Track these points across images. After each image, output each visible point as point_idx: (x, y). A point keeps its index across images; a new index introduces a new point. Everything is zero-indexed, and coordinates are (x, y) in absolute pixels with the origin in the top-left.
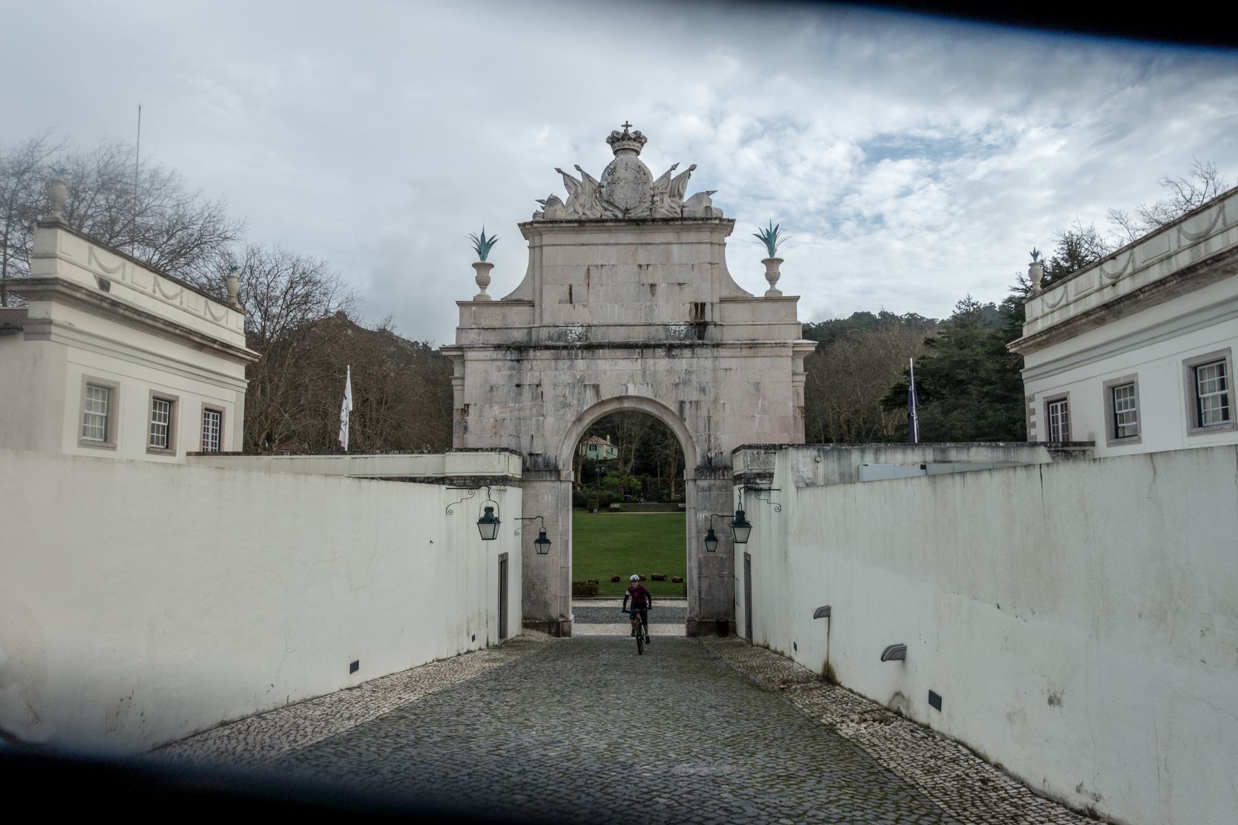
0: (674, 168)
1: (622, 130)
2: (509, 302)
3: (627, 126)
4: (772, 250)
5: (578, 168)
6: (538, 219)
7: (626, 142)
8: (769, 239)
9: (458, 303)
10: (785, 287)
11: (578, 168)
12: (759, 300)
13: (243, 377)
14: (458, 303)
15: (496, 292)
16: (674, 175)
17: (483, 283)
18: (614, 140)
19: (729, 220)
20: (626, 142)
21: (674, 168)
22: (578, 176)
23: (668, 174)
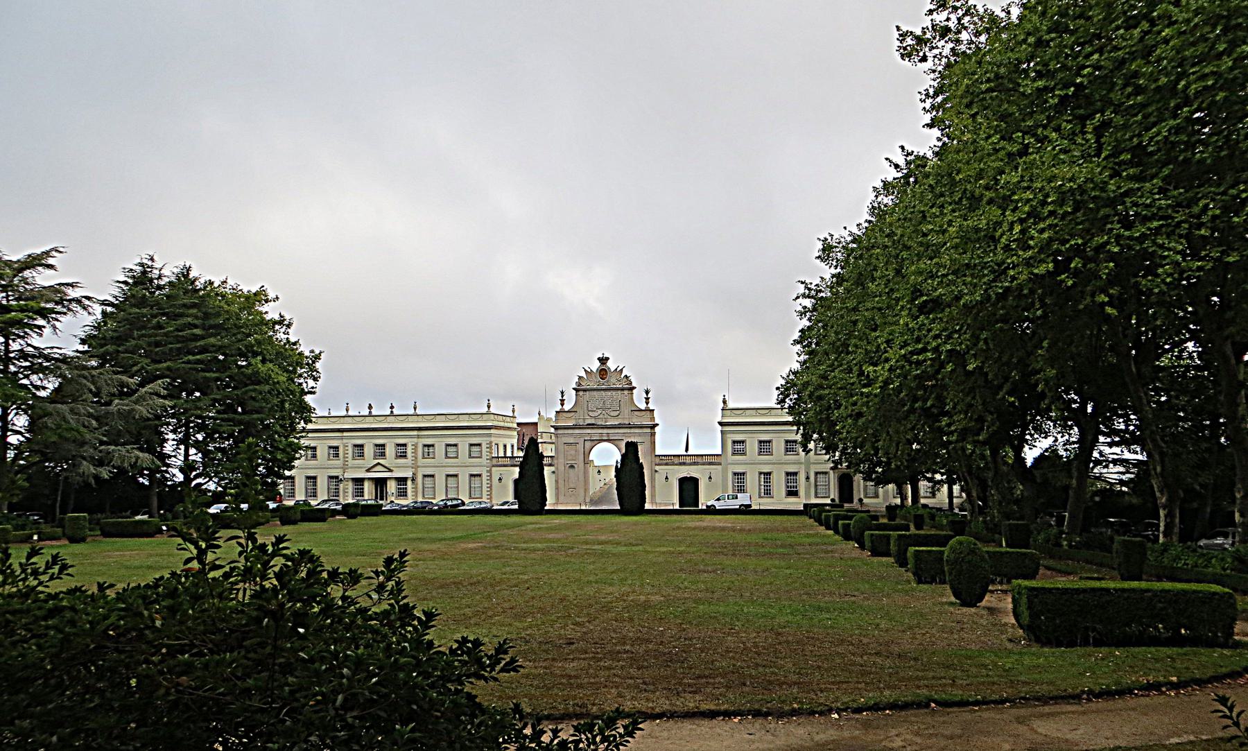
7: (603, 360)
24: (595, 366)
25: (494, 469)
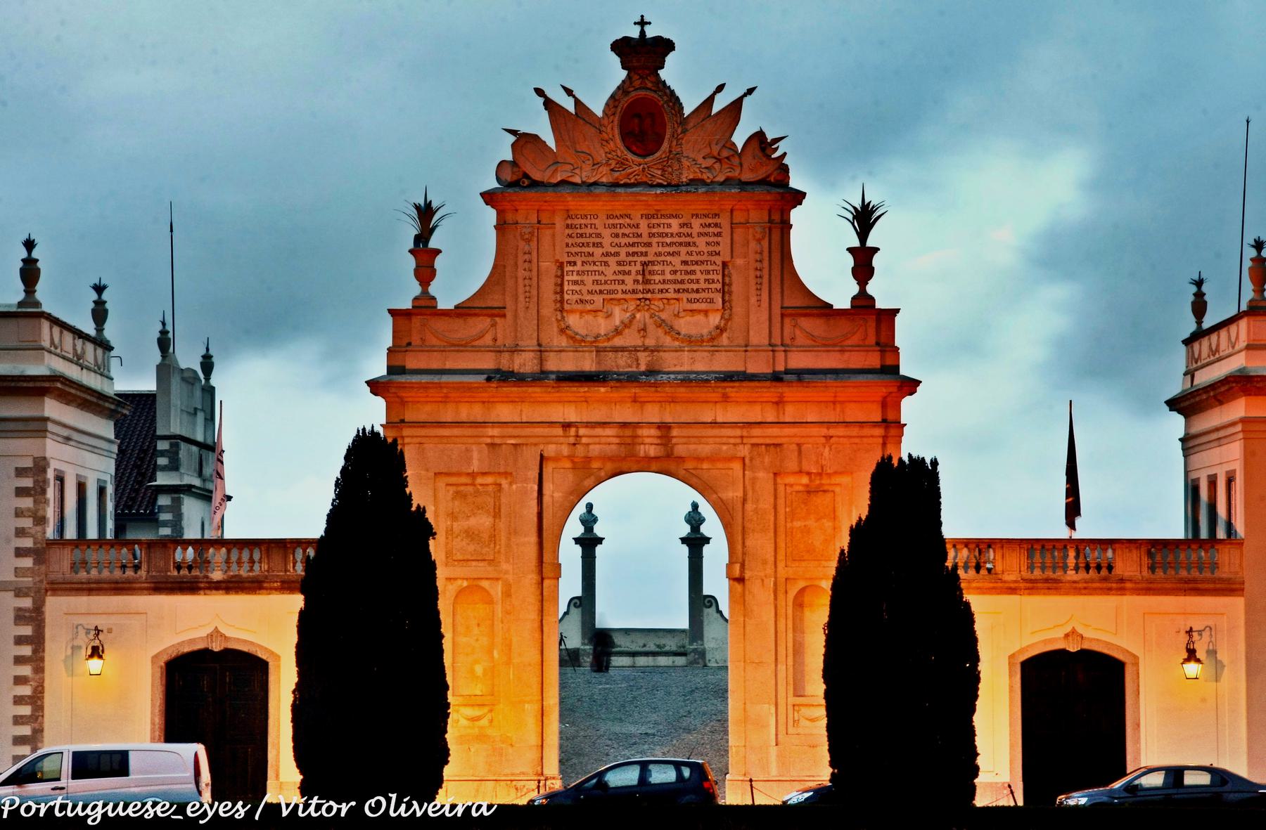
0: (720, 88)
1: (634, 33)
2: (463, 311)
3: (642, 23)
4: (863, 234)
5: (569, 92)
6: (508, 177)
7: (644, 53)
8: (864, 218)
9: (390, 311)
10: (881, 291)
11: (569, 92)
12: (842, 312)
13: (112, 437)
14: (390, 311)
15: (451, 290)
16: (718, 106)
17: (425, 273)
18: (622, 47)
19: (720, 668)
20: (644, 53)
21: (720, 88)
22: (569, 105)
23: (710, 101)
24: (600, 82)
25: (55, 605)
